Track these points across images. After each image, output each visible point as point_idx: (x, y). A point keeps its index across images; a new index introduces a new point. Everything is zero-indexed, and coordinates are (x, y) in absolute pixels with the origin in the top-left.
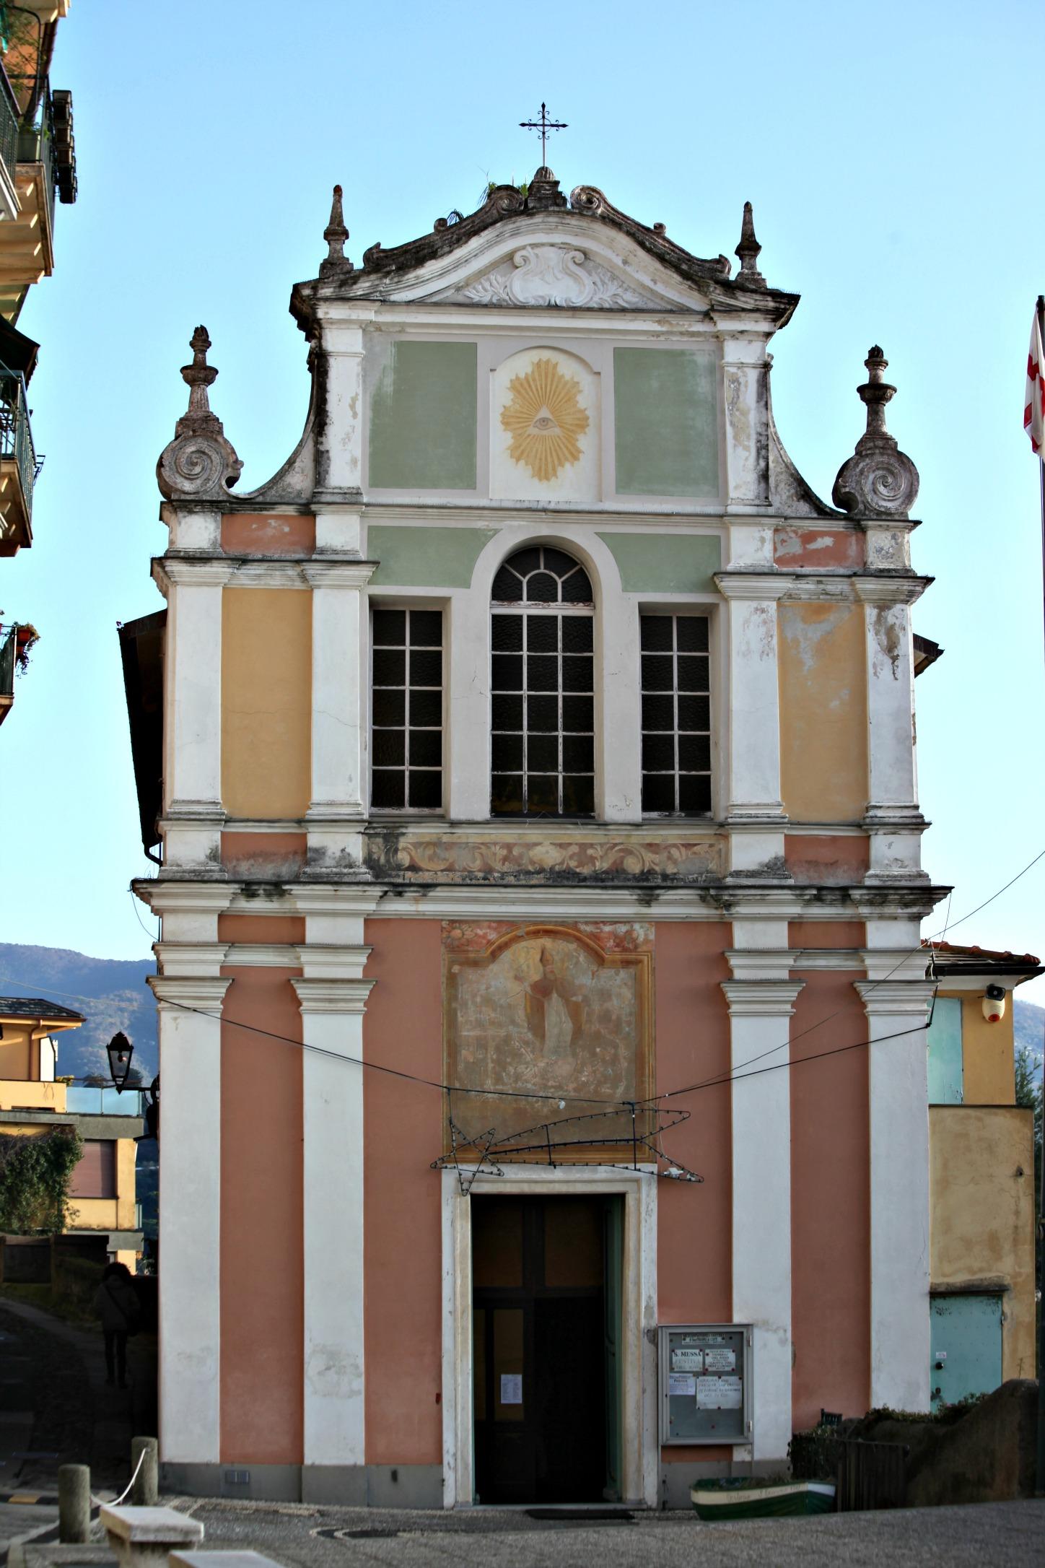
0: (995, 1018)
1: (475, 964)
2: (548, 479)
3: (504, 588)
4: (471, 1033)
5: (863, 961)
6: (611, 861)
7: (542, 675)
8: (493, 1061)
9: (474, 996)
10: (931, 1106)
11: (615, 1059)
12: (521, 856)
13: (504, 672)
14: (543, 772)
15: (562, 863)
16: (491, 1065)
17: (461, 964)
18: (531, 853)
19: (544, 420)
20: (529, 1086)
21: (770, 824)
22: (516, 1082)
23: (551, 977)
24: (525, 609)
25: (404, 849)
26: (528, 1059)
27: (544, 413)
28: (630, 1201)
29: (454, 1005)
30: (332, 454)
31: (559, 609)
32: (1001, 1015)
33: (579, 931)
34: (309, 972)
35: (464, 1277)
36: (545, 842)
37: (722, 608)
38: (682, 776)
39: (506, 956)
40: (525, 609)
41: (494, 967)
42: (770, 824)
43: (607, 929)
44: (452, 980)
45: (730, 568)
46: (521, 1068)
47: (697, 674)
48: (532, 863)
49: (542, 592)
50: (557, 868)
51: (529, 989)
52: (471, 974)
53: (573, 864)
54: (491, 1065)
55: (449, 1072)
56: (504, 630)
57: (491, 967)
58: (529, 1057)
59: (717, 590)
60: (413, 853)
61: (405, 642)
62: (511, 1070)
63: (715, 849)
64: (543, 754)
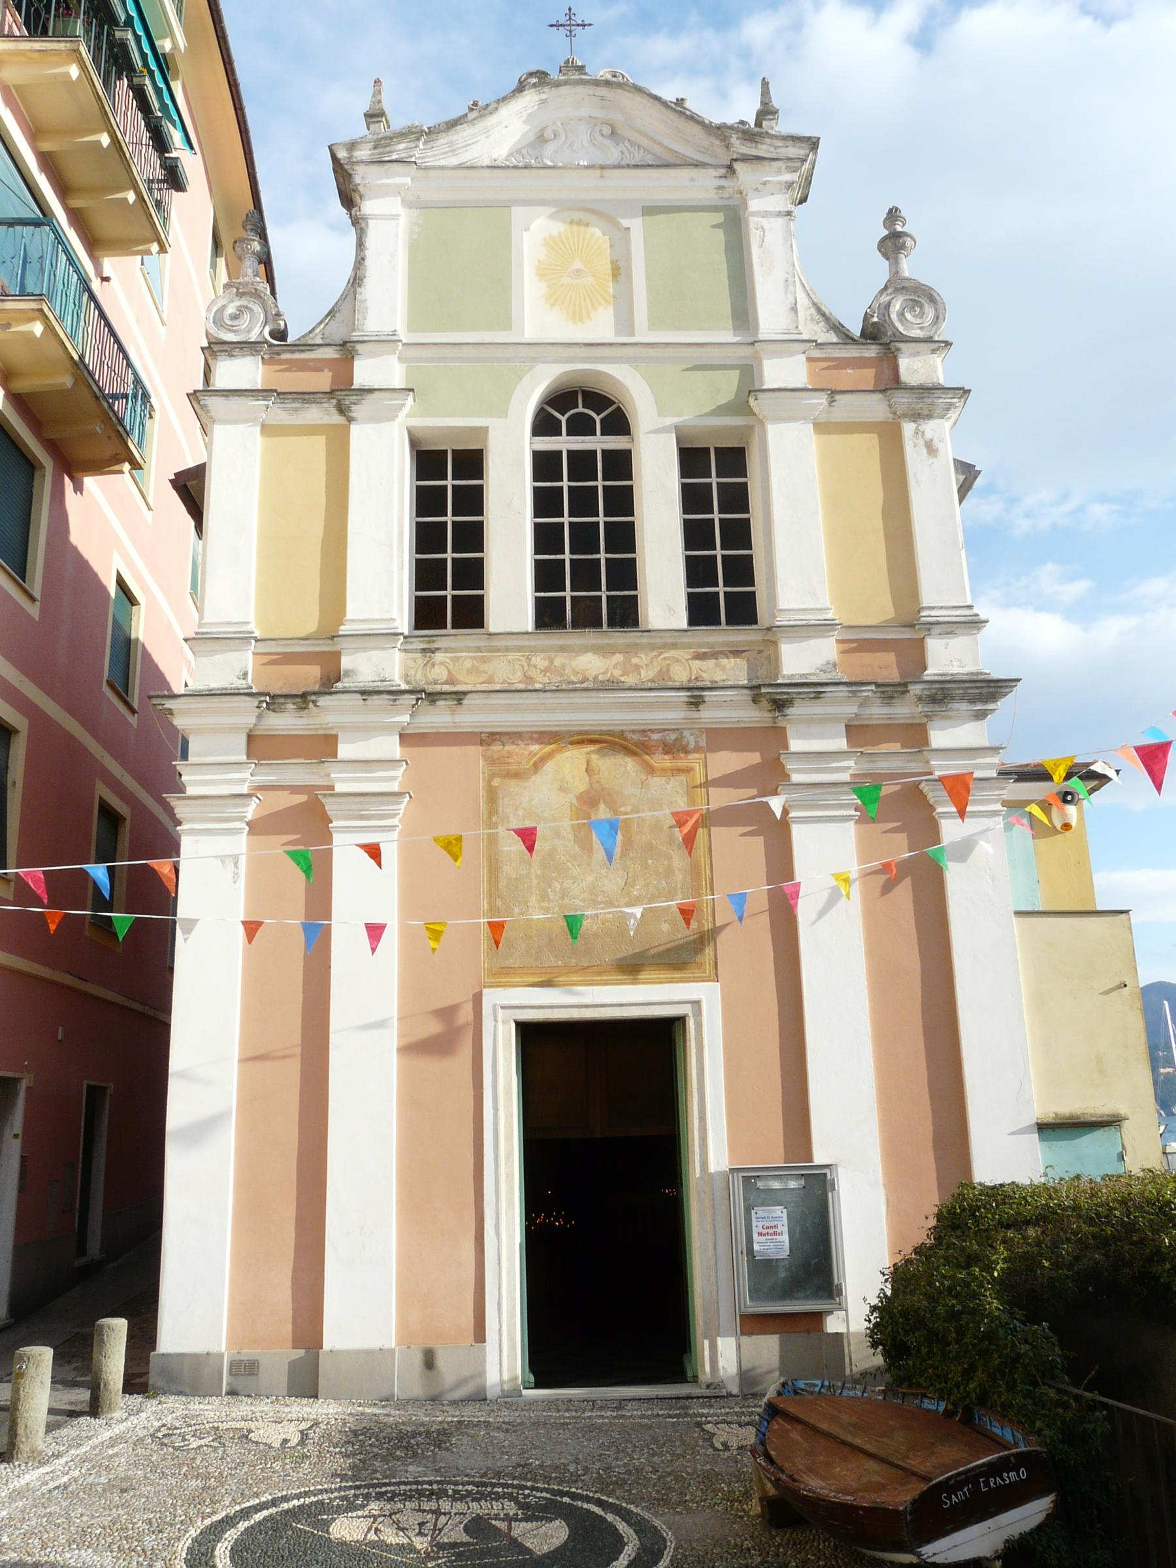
0: (1067, 826)
1: (517, 775)
2: (581, 321)
3: (544, 425)
4: (512, 848)
5: (928, 762)
6: (657, 669)
7: (586, 575)
8: (537, 877)
9: (517, 809)
10: (1018, 913)
11: (669, 872)
12: (563, 667)
13: (545, 502)
14: (587, 582)
15: (605, 673)
16: (535, 881)
17: (503, 776)
18: (574, 663)
19: (577, 271)
20: (577, 902)
21: (823, 628)
22: (563, 898)
23: (596, 786)
24: (564, 443)
25: (441, 663)
26: (575, 873)
27: (577, 265)
28: (691, 1024)
29: (494, 819)
30: (369, 304)
31: (598, 443)
32: (1074, 823)
33: (625, 739)
34: (339, 788)
35: (509, 1116)
36: (588, 656)
37: (757, 430)
38: (725, 584)
39: (550, 766)
40: (564, 443)
41: (536, 779)
42: (823, 628)
43: (656, 736)
44: (492, 796)
45: (765, 387)
46: (568, 883)
47: (737, 498)
48: (576, 673)
49: (581, 427)
50: (601, 678)
51: (574, 802)
52: (513, 786)
53: (617, 673)
54: (535, 881)
55: (490, 890)
56: (545, 465)
57: (533, 778)
58: (576, 871)
59: (751, 413)
60: (451, 667)
61: (447, 481)
62: (557, 885)
63: (765, 654)
64: (584, 538)
